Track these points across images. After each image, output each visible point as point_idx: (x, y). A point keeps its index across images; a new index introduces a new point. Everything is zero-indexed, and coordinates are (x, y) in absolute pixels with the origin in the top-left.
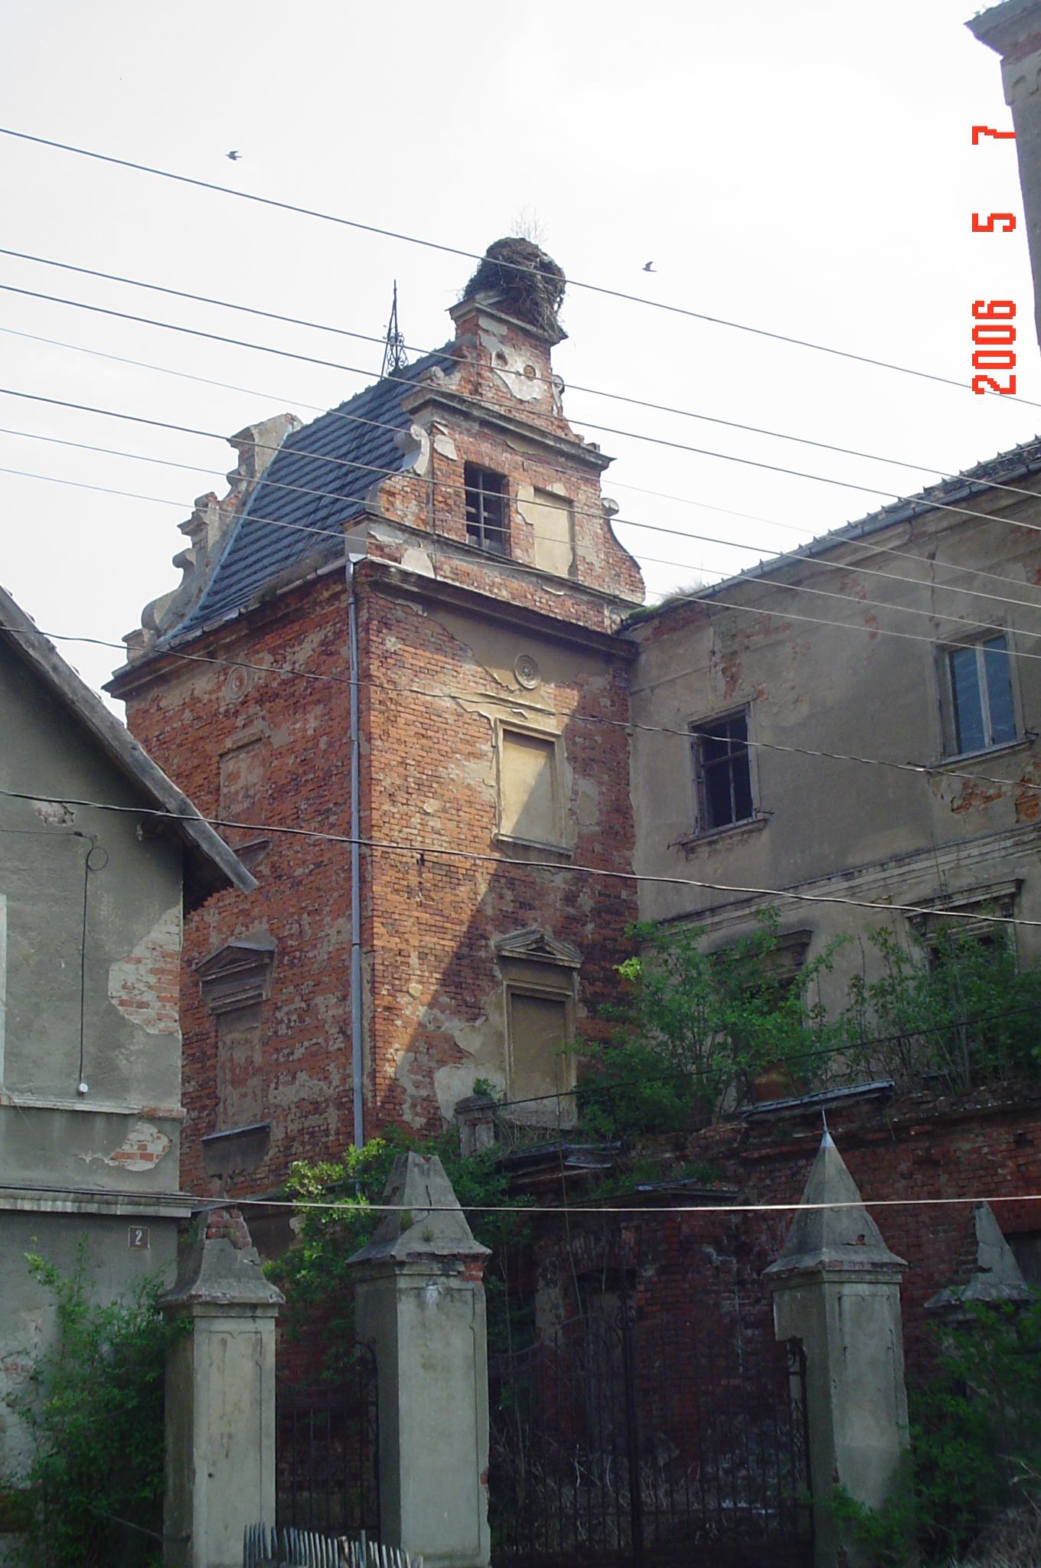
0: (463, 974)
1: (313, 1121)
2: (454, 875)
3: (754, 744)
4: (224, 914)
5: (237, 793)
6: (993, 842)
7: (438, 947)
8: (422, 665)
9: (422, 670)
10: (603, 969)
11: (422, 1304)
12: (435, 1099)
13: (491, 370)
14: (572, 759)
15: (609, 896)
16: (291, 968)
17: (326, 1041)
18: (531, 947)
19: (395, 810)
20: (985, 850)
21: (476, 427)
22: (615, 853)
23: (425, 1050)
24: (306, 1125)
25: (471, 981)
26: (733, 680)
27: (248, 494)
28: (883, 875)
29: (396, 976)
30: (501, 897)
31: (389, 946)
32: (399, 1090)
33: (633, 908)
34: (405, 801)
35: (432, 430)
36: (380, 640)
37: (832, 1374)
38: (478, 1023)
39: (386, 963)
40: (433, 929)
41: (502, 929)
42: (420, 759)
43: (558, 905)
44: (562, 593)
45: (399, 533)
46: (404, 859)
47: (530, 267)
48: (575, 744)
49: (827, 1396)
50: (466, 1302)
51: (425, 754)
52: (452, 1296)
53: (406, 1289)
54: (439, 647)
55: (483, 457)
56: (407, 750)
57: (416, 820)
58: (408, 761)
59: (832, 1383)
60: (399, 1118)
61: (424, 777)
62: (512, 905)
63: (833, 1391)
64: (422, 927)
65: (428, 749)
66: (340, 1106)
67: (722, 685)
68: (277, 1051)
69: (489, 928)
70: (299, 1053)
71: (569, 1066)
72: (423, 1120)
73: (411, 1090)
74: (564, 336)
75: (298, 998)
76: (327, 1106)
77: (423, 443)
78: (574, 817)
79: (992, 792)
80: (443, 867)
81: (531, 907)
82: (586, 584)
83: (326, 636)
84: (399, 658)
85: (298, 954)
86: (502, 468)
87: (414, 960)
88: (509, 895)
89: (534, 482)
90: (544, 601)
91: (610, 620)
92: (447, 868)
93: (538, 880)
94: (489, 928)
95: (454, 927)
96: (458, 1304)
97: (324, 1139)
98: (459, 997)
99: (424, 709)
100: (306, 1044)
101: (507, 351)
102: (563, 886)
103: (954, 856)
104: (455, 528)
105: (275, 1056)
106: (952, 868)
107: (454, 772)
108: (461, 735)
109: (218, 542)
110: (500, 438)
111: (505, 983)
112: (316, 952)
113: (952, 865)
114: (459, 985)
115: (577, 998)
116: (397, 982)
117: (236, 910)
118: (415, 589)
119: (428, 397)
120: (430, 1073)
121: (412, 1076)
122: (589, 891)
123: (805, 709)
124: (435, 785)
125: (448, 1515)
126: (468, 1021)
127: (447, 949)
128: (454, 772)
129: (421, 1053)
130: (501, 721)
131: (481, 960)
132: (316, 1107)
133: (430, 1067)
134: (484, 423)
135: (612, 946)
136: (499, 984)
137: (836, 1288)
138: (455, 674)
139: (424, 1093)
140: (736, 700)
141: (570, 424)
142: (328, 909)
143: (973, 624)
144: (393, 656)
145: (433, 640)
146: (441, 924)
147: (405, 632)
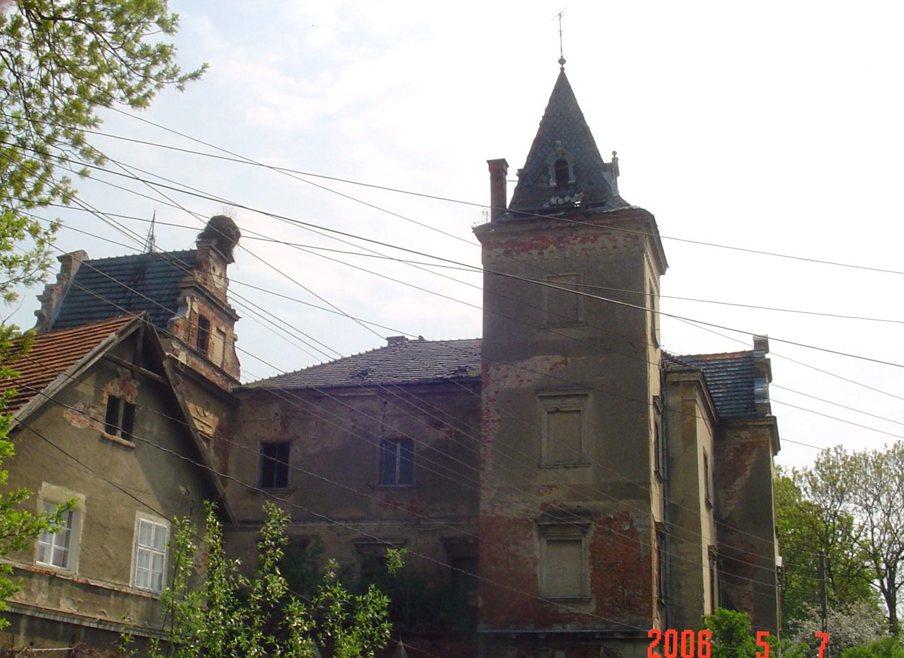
13: (211, 274)
14: (214, 447)
21: (204, 299)
26: (285, 429)
27: (66, 287)
35: (192, 299)
44: (219, 375)
45: (179, 344)
47: (234, 233)
67: (279, 429)
74: (233, 261)
79: (398, 502)
91: (230, 387)
109: (509, 519)
110: (210, 304)
118: (183, 370)
119: (194, 285)
123: (318, 449)
134: (207, 298)
140: (286, 437)
141: (228, 298)
143: (399, 433)
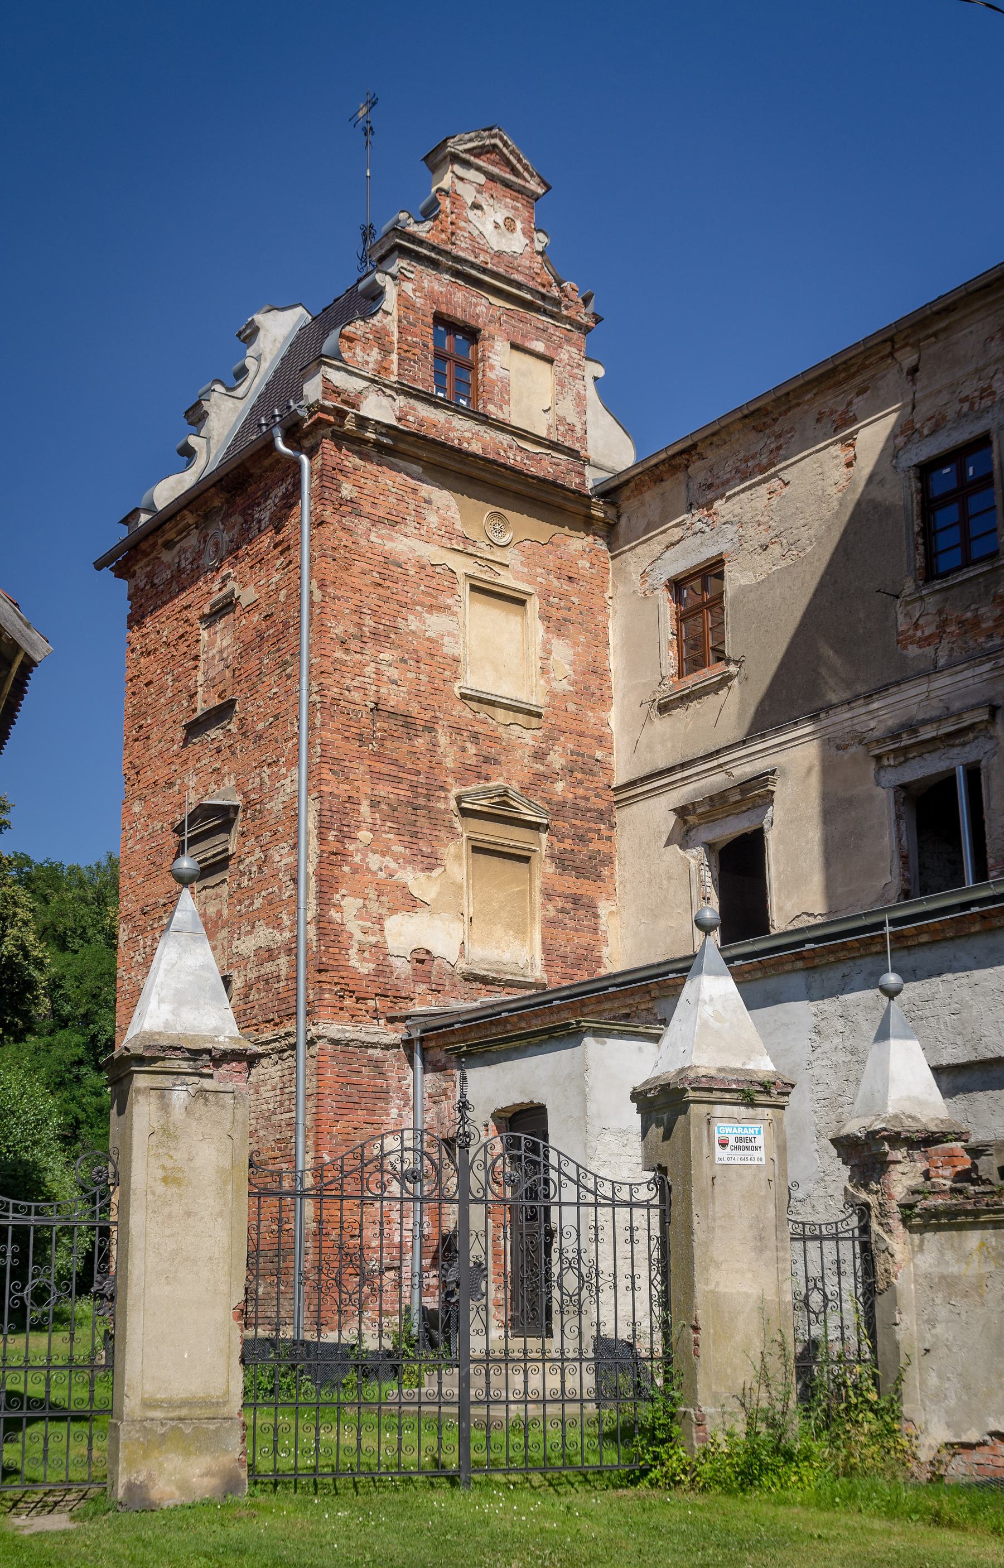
0: (418, 824)
1: (269, 968)
2: (413, 726)
3: (730, 589)
4: (201, 775)
5: (213, 657)
6: (966, 669)
7: (392, 796)
8: (382, 515)
9: (381, 520)
10: (573, 826)
11: (165, 1108)
12: (386, 946)
15: (583, 756)
16: (253, 820)
17: (280, 889)
18: (493, 801)
19: (348, 658)
20: (959, 678)
22: (591, 714)
23: (376, 897)
24: (262, 972)
25: (428, 832)
28: (849, 715)
29: (344, 822)
30: (464, 750)
31: (336, 791)
32: (345, 935)
33: (606, 768)
34: (359, 650)
36: (335, 487)
37: (695, 1209)
38: (435, 874)
39: (334, 809)
40: (387, 778)
41: (463, 782)
42: (377, 608)
43: (526, 761)
46: (357, 707)
48: (549, 604)
49: (690, 1232)
50: (223, 1107)
51: (381, 604)
52: (206, 1099)
53: (145, 1088)
54: (400, 498)
55: (455, 309)
56: (363, 598)
57: (370, 670)
58: (364, 610)
59: (695, 1218)
60: (345, 963)
61: (381, 627)
62: (475, 758)
63: (695, 1225)
64: (375, 775)
65: (386, 599)
66: (289, 951)
68: (240, 902)
69: (450, 780)
70: (258, 903)
71: (533, 919)
72: (372, 966)
73: (358, 936)
75: (258, 850)
76: (279, 953)
77: (387, 289)
78: (546, 676)
80: (399, 717)
81: (496, 762)
82: (566, 444)
83: (287, 489)
84: (355, 506)
85: (258, 807)
86: (477, 321)
87: (365, 808)
88: (472, 749)
89: (511, 337)
90: (518, 459)
92: (403, 719)
93: (504, 736)
94: (450, 780)
95: (410, 777)
96: (213, 1109)
97: (276, 986)
98: (415, 846)
99: (383, 559)
100: (264, 893)
101: (483, 200)
102: (531, 743)
103: (924, 688)
104: (423, 377)
105: (238, 908)
106: (922, 701)
107: (413, 624)
108: (422, 588)
111: (465, 835)
112: (272, 804)
113: (923, 697)
114: (414, 835)
115: (544, 853)
116: (345, 829)
117: (210, 770)
120: (381, 918)
121: (360, 922)
122: (560, 749)
124: (392, 636)
125: (189, 1356)
126: (423, 870)
127: (402, 798)
128: (413, 624)
129: (370, 899)
130: (467, 575)
131: (439, 811)
132: (270, 954)
133: (380, 914)
135: (584, 804)
136: (459, 836)
137: (704, 1108)
138: (418, 526)
139: (373, 939)
142: (284, 759)
144: (349, 503)
145: (394, 490)
146: (396, 774)
147: (363, 480)
